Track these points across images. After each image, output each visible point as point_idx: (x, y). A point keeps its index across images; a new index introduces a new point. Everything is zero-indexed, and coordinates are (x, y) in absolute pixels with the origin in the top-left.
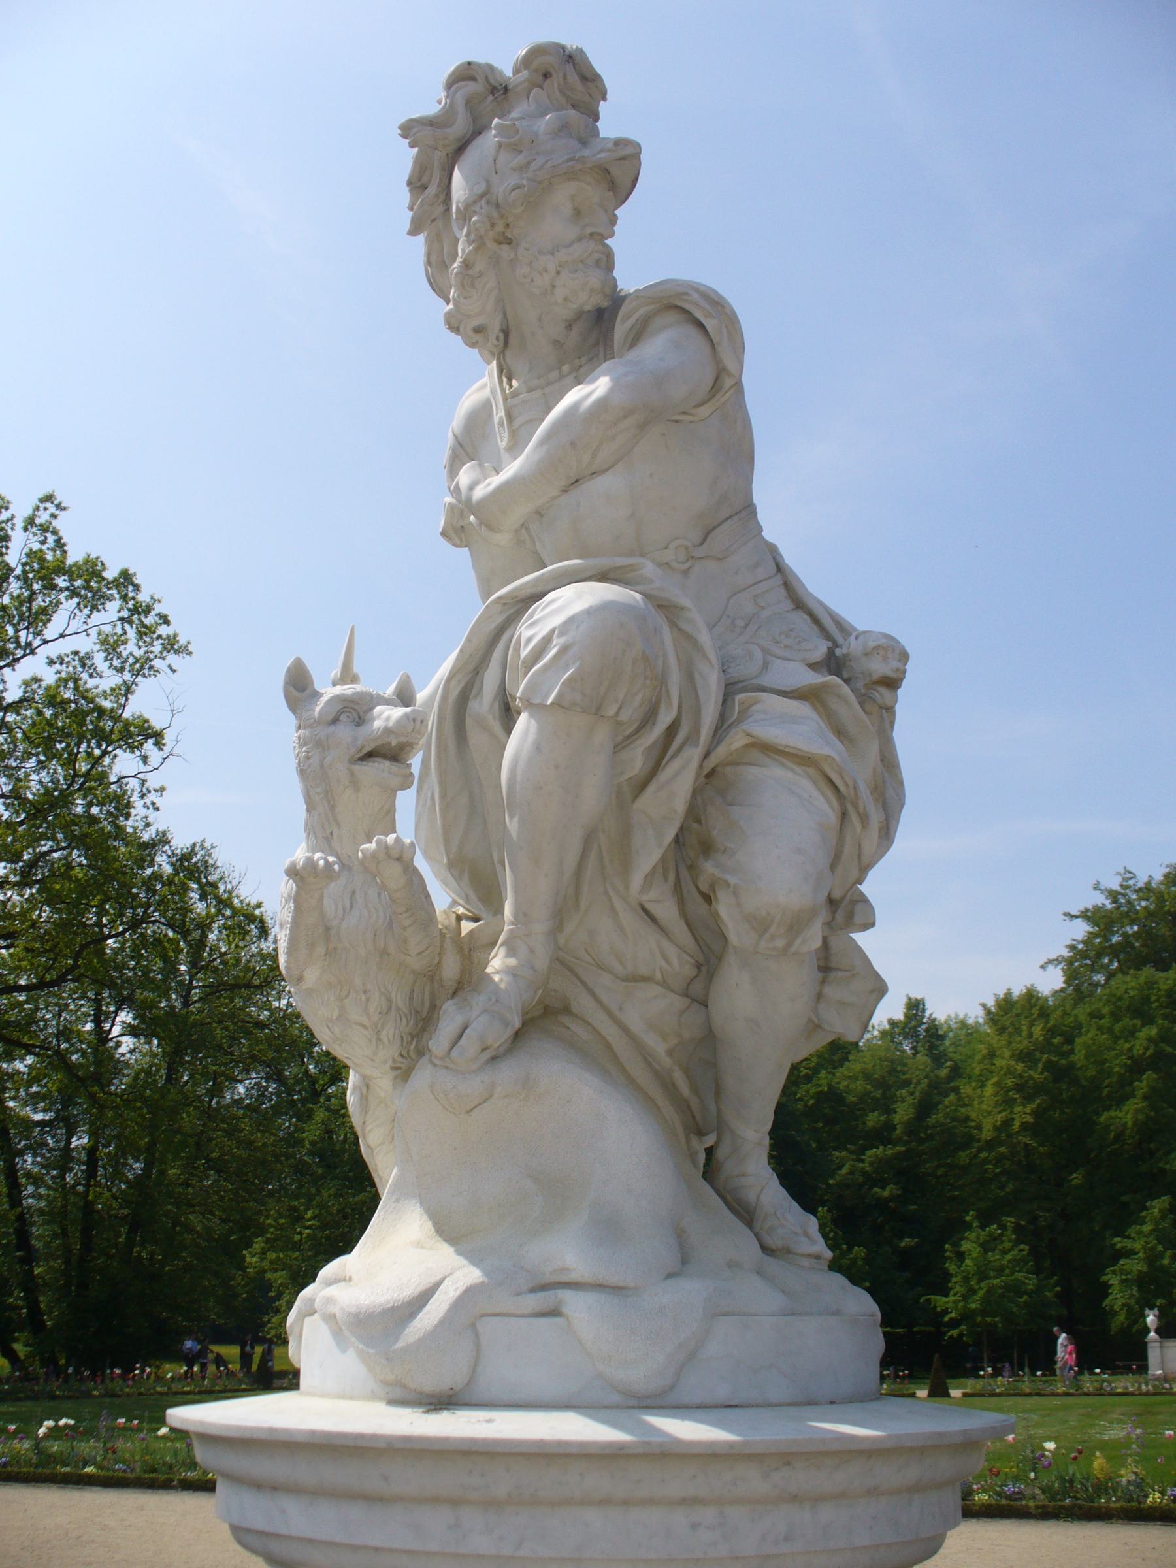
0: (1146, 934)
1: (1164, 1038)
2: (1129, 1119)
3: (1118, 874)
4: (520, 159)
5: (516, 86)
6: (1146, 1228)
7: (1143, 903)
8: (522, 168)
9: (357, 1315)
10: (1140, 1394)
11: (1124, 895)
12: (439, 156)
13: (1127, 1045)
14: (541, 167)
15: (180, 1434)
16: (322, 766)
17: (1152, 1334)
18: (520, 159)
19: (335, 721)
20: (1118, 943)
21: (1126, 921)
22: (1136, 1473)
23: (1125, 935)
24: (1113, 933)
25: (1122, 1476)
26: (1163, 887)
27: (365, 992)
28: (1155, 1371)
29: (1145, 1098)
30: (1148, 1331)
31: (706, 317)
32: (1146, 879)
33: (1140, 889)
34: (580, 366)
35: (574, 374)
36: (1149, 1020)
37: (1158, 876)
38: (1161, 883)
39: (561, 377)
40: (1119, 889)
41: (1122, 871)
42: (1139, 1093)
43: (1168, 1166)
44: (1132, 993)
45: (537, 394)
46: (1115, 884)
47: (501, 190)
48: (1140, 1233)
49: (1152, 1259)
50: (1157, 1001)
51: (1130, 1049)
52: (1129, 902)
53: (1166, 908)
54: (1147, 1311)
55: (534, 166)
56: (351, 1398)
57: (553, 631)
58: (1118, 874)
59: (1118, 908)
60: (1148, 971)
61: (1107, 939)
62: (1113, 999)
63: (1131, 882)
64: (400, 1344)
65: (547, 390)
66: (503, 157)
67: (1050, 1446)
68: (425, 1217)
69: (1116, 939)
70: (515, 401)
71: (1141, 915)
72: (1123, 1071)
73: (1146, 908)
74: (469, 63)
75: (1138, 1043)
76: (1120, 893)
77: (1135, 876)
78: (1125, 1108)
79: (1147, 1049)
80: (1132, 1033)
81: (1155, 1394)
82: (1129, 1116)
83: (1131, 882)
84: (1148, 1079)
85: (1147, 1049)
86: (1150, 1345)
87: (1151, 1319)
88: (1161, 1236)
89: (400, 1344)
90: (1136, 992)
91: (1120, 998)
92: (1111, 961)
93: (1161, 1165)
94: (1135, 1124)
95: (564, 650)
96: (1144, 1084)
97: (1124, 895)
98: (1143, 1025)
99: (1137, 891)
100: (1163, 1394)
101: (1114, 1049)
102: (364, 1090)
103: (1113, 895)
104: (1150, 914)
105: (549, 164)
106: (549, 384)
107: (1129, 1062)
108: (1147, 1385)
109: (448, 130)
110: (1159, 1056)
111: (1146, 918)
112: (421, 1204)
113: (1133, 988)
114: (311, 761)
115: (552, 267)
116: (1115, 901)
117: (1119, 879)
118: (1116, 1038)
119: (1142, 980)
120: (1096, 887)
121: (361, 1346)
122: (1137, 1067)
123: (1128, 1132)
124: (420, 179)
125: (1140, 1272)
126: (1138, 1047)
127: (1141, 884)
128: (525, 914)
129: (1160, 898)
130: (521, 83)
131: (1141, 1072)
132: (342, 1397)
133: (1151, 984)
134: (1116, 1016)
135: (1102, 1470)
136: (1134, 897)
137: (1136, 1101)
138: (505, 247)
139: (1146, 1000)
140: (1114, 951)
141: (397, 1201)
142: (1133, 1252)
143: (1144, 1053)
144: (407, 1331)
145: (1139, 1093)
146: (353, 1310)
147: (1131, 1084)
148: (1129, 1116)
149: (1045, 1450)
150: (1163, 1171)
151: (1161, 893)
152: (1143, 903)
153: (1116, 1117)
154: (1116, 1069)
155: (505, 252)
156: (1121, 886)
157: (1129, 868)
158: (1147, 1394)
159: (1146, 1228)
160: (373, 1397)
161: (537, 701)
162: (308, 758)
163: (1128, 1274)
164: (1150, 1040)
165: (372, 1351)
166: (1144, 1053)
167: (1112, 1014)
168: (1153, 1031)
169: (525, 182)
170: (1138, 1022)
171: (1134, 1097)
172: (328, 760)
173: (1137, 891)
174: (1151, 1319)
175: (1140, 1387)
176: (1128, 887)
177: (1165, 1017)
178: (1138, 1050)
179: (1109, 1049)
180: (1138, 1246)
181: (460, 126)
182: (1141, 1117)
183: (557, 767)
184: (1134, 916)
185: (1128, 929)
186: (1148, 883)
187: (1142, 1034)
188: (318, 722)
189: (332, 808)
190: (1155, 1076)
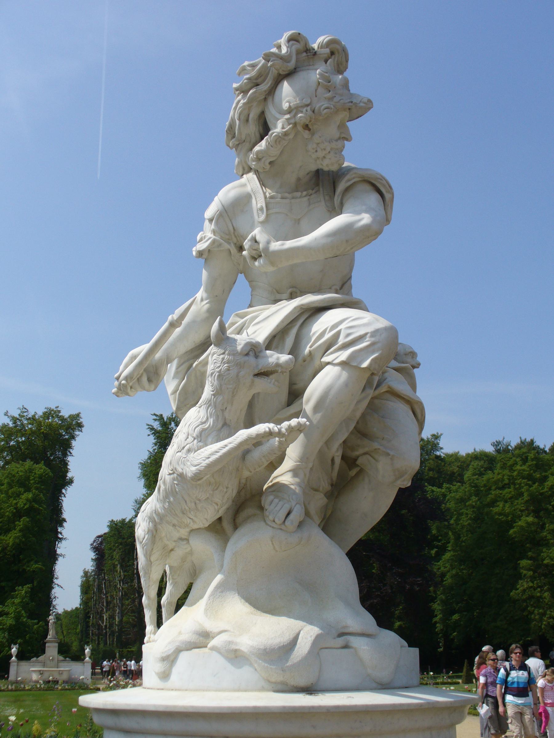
0: (29, 443)
1: (35, 500)
2: (11, 542)
3: (19, 408)
4: (329, 95)
5: (320, 54)
6: (17, 601)
7: (30, 426)
8: (331, 99)
9: (265, 650)
10: (8, 691)
11: (20, 421)
12: (273, 73)
13: (15, 502)
14: (338, 102)
15: (85, 710)
16: (237, 376)
17: (14, 658)
18: (329, 95)
19: (247, 354)
20: (13, 446)
21: (19, 434)
22: (55, 732)
23: (18, 442)
24: (11, 440)
25: (47, 733)
26: (41, 419)
27: (227, 488)
28: (12, 677)
29: (20, 531)
30: (11, 656)
31: (386, 192)
32: (33, 414)
33: (29, 418)
34: (311, 194)
35: (308, 197)
36: (28, 490)
37: (40, 413)
38: (41, 417)
39: (301, 197)
40: (18, 417)
41: (21, 407)
42: (18, 528)
43: (28, 568)
44: (21, 474)
45: (287, 201)
46: (16, 414)
47: (318, 106)
48: (14, 603)
49: (17, 618)
50: (34, 479)
51: (16, 504)
52: (22, 424)
53: (42, 431)
54: (12, 646)
55: (336, 100)
56: (246, 691)
57: (366, 334)
58: (19, 408)
59: (16, 427)
60: (28, 463)
61: (8, 443)
62: (10, 476)
63: (25, 414)
64: (289, 663)
65: (293, 201)
66: (320, 90)
67: (13, 718)
68: (243, 600)
69: (12, 443)
70: (272, 201)
71: (28, 432)
72: (11, 515)
73: (31, 429)
74: (299, 34)
75: (21, 501)
76: (18, 419)
77: (28, 411)
78: (10, 535)
79: (25, 504)
80: (18, 495)
81: (16, 690)
82: (11, 540)
83: (25, 414)
84: (24, 520)
85: (25, 504)
86: (11, 664)
87: (14, 650)
88: (24, 606)
89: (289, 663)
90: (23, 474)
91: (14, 476)
92: (8, 455)
93: (25, 567)
94: (13, 544)
95: (373, 344)
96: (21, 523)
97: (20, 421)
98: (25, 492)
99: (27, 419)
100: (20, 690)
101: (7, 503)
102: (155, 532)
103: (14, 420)
104: (33, 433)
105: (342, 101)
106: (293, 198)
107: (15, 511)
108: (12, 686)
109: (288, 64)
110: (31, 508)
111: (30, 435)
112: (238, 593)
113: (21, 471)
114: (231, 372)
115: (328, 149)
116: (15, 423)
117: (19, 412)
118: (9, 497)
119: (27, 467)
120: (6, 414)
121: (266, 665)
122: (18, 514)
123: (8, 548)
124: (257, 79)
125: (11, 624)
126: (20, 503)
127: (30, 416)
128: (307, 458)
129: (39, 424)
130: (325, 54)
131: (21, 517)
132: (239, 690)
133: (31, 471)
134: (10, 486)
135: (37, 730)
136: (26, 422)
137: (15, 532)
138: (307, 132)
139: (28, 478)
140: (11, 449)
141: (222, 592)
142: (7, 614)
143: (24, 507)
144: (292, 657)
145: (18, 528)
146: (262, 647)
147: (14, 522)
148: (11, 540)
149: (9, 721)
150: (24, 570)
151: (40, 422)
152: (30, 426)
153: (3, 540)
154: (7, 514)
155: (306, 134)
156: (19, 415)
157: (25, 406)
158: (12, 690)
159: (17, 601)
160: (263, 689)
161: (355, 364)
162: (229, 370)
163: (4, 625)
164: (27, 500)
165: (273, 667)
166: (24, 507)
167: (8, 483)
168: (30, 495)
169: (332, 106)
170: (22, 490)
171: (15, 530)
172: (242, 373)
173: (27, 419)
174: (14, 650)
175: (8, 687)
176: (24, 416)
177: (37, 489)
178: (21, 504)
179: (4, 502)
180: (11, 610)
181: (292, 65)
182: (17, 541)
183: (352, 395)
184: (24, 432)
185: (20, 439)
186: (34, 416)
187: (24, 497)
188: (240, 354)
189: (233, 396)
190: (28, 519)
